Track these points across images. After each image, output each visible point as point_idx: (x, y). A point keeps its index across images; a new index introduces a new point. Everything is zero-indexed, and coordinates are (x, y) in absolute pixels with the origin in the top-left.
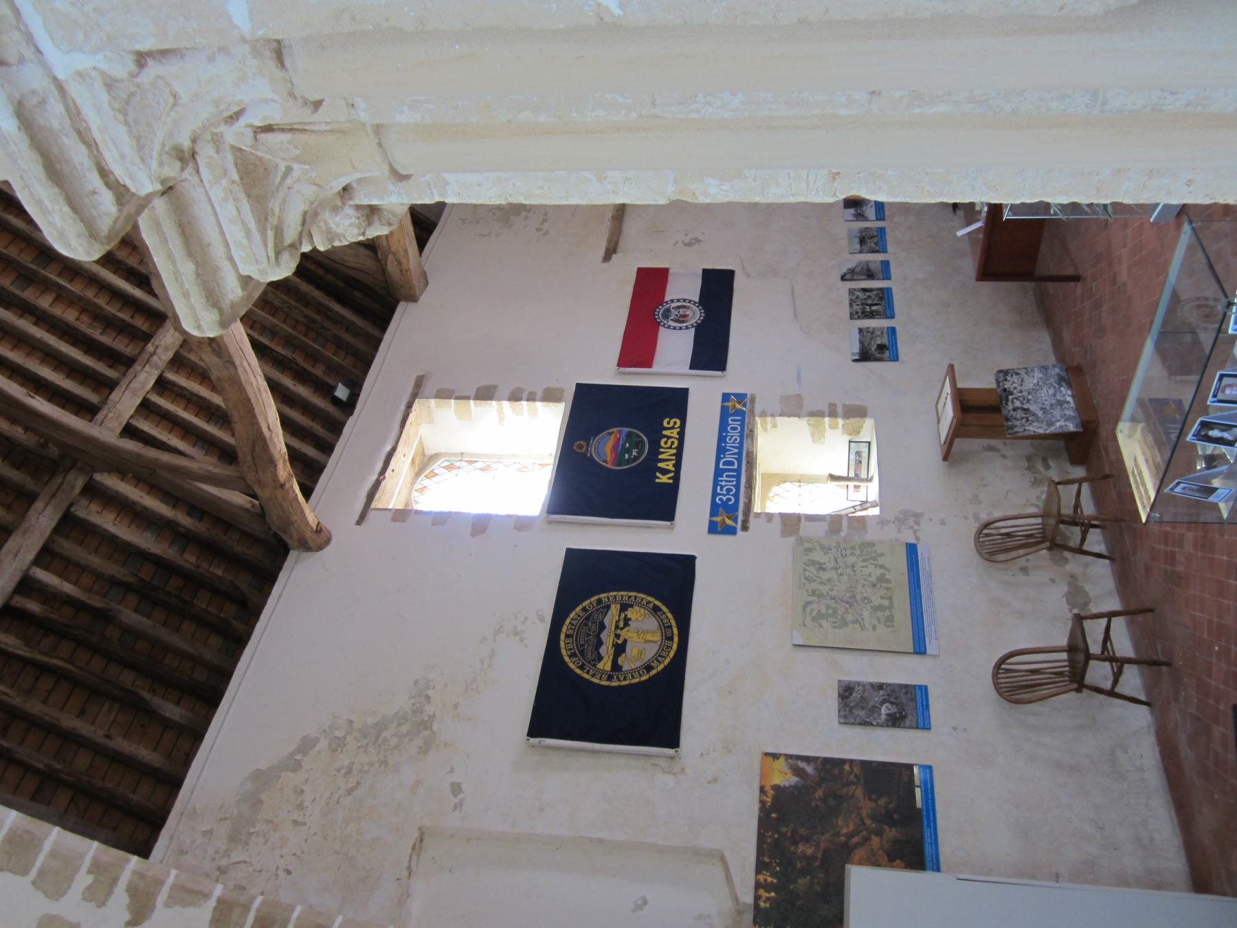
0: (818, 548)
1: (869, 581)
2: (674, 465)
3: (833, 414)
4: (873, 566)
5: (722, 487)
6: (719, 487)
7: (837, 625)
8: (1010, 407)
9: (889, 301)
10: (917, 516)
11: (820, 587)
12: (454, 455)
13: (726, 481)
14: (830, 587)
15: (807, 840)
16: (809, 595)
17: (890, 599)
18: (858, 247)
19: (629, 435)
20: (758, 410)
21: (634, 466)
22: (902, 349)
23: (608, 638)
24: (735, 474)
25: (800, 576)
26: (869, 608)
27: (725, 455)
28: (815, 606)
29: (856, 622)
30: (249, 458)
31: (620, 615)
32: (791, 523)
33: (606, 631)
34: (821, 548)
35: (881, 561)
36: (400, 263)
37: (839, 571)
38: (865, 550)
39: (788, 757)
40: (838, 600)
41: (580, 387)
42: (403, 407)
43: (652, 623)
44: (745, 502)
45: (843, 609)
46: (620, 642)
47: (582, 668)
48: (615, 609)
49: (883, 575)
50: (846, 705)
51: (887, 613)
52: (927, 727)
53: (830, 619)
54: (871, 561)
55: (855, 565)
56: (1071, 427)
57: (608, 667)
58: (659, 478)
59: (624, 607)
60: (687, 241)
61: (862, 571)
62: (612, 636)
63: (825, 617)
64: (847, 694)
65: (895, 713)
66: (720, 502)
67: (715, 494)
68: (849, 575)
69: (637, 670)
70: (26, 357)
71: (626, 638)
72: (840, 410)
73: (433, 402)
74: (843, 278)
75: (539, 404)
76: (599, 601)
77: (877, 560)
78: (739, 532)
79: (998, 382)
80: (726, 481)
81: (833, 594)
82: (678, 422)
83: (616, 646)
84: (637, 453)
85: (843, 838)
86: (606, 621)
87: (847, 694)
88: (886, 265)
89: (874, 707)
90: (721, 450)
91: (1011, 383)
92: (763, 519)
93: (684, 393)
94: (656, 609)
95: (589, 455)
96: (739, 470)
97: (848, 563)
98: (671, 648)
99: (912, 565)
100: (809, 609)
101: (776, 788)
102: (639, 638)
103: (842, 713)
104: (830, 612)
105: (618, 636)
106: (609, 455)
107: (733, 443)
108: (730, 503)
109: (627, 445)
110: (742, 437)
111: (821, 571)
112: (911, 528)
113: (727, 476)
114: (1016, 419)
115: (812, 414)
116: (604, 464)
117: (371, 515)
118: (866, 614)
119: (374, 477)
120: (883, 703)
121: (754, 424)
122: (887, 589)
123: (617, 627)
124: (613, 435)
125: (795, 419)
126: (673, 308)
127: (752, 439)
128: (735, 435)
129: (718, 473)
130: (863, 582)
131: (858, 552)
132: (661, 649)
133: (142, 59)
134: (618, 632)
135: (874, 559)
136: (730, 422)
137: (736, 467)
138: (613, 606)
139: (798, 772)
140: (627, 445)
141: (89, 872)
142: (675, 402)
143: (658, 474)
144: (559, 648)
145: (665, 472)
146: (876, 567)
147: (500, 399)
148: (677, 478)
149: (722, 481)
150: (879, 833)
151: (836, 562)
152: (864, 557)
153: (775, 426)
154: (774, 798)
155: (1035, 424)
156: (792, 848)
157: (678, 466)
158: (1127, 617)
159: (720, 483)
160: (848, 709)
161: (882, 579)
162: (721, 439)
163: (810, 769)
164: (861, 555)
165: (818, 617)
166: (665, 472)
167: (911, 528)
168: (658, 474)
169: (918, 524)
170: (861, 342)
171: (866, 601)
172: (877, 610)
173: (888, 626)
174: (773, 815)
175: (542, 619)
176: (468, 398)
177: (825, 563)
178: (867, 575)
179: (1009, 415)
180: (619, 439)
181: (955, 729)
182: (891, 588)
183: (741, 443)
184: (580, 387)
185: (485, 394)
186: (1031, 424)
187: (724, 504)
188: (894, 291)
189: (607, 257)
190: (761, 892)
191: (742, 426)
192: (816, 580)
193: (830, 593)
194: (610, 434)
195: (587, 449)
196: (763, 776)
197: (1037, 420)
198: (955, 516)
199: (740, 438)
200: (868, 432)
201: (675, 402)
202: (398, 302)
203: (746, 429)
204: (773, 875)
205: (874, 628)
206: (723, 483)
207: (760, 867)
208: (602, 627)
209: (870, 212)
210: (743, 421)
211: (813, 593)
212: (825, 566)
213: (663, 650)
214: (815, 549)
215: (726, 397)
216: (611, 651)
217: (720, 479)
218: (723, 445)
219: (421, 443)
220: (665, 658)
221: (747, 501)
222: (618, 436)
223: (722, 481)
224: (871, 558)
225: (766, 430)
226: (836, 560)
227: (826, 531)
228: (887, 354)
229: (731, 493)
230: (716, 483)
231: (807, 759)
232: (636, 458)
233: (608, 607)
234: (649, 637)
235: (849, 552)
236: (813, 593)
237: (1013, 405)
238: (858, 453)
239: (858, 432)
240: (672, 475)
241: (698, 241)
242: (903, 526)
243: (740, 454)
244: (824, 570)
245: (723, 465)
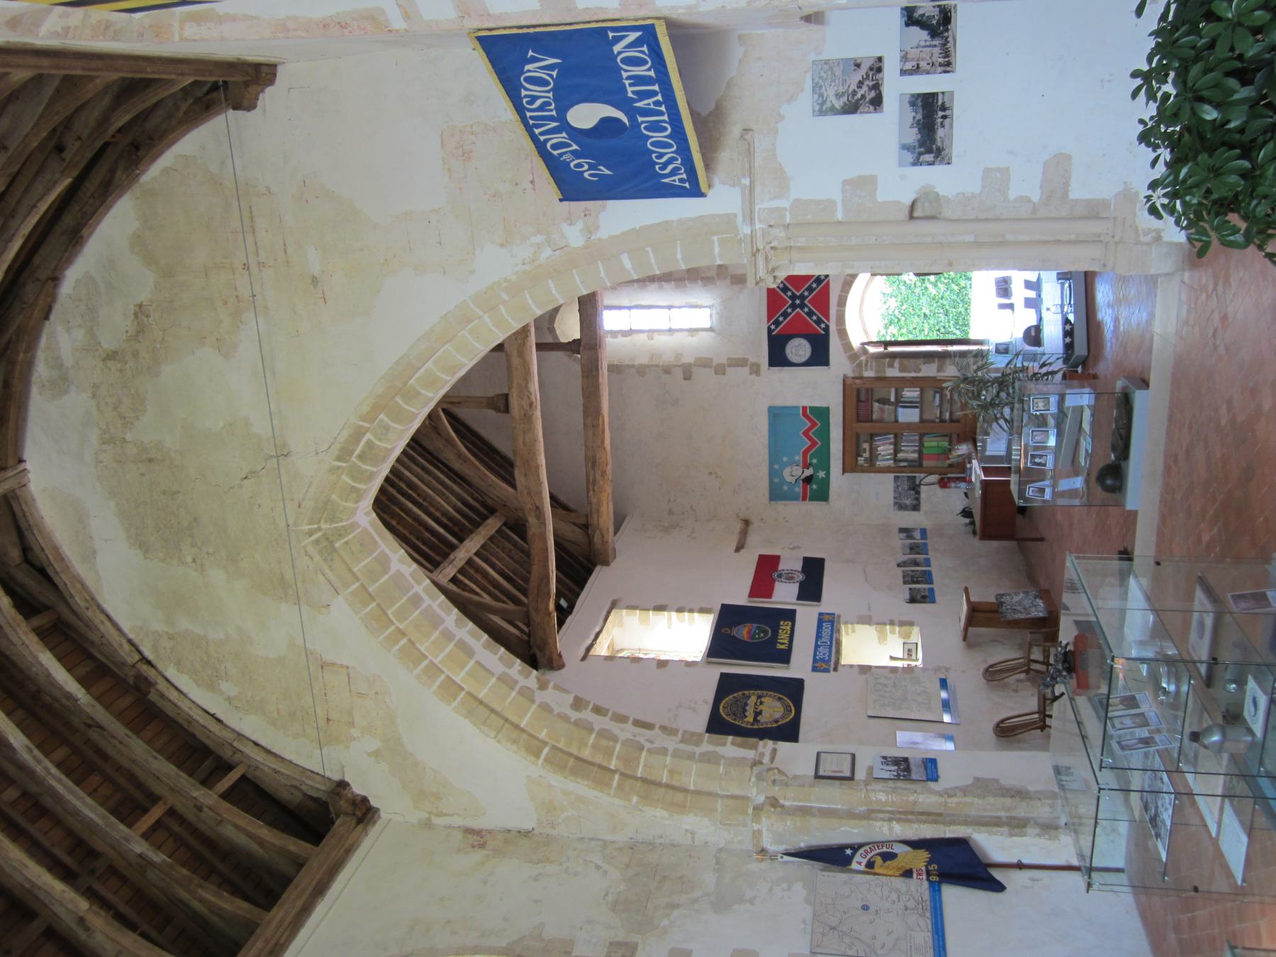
3: (892, 623)
12: (635, 650)
18: (909, 551)
19: (758, 628)
22: (937, 598)
30: (536, 591)
32: (865, 669)
36: (603, 537)
41: (724, 606)
42: (604, 613)
56: (1041, 615)
57: (751, 720)
59: (759, 697)
60: (791, 547)
70: (904, 147)
72: (896, 622)
73: (624, 611)
74: (899, 565)
75: (696, 615)
76: (744, 694)
79: (997, 599)
82: (790, 623)
91: (1006, 599)
93: (794, 611)
94: (780, 699)
115: (878, 624)
117: (588, 657)
119: (589, 642)
125: (867, 626)
133: (770, 226)
142: (790, 615)
147: (670, 610)
153: (853, 631)
176: (648, 610)
184: (724, 606)
185: (660, 608)
188: (933, 572)
189: (738, 549)
200: (916, 636)
201: (790, 615)
202: (595, 566)
208: (746, 704)
209: (917, 535)
215: (821, 614)
216: (753, 715)
219: (612, 639)
225: (847, 634)
228: (928, 599)
230: (816, 650)
238: (909, 650)
239: (908, 636)
241: (799, 547)
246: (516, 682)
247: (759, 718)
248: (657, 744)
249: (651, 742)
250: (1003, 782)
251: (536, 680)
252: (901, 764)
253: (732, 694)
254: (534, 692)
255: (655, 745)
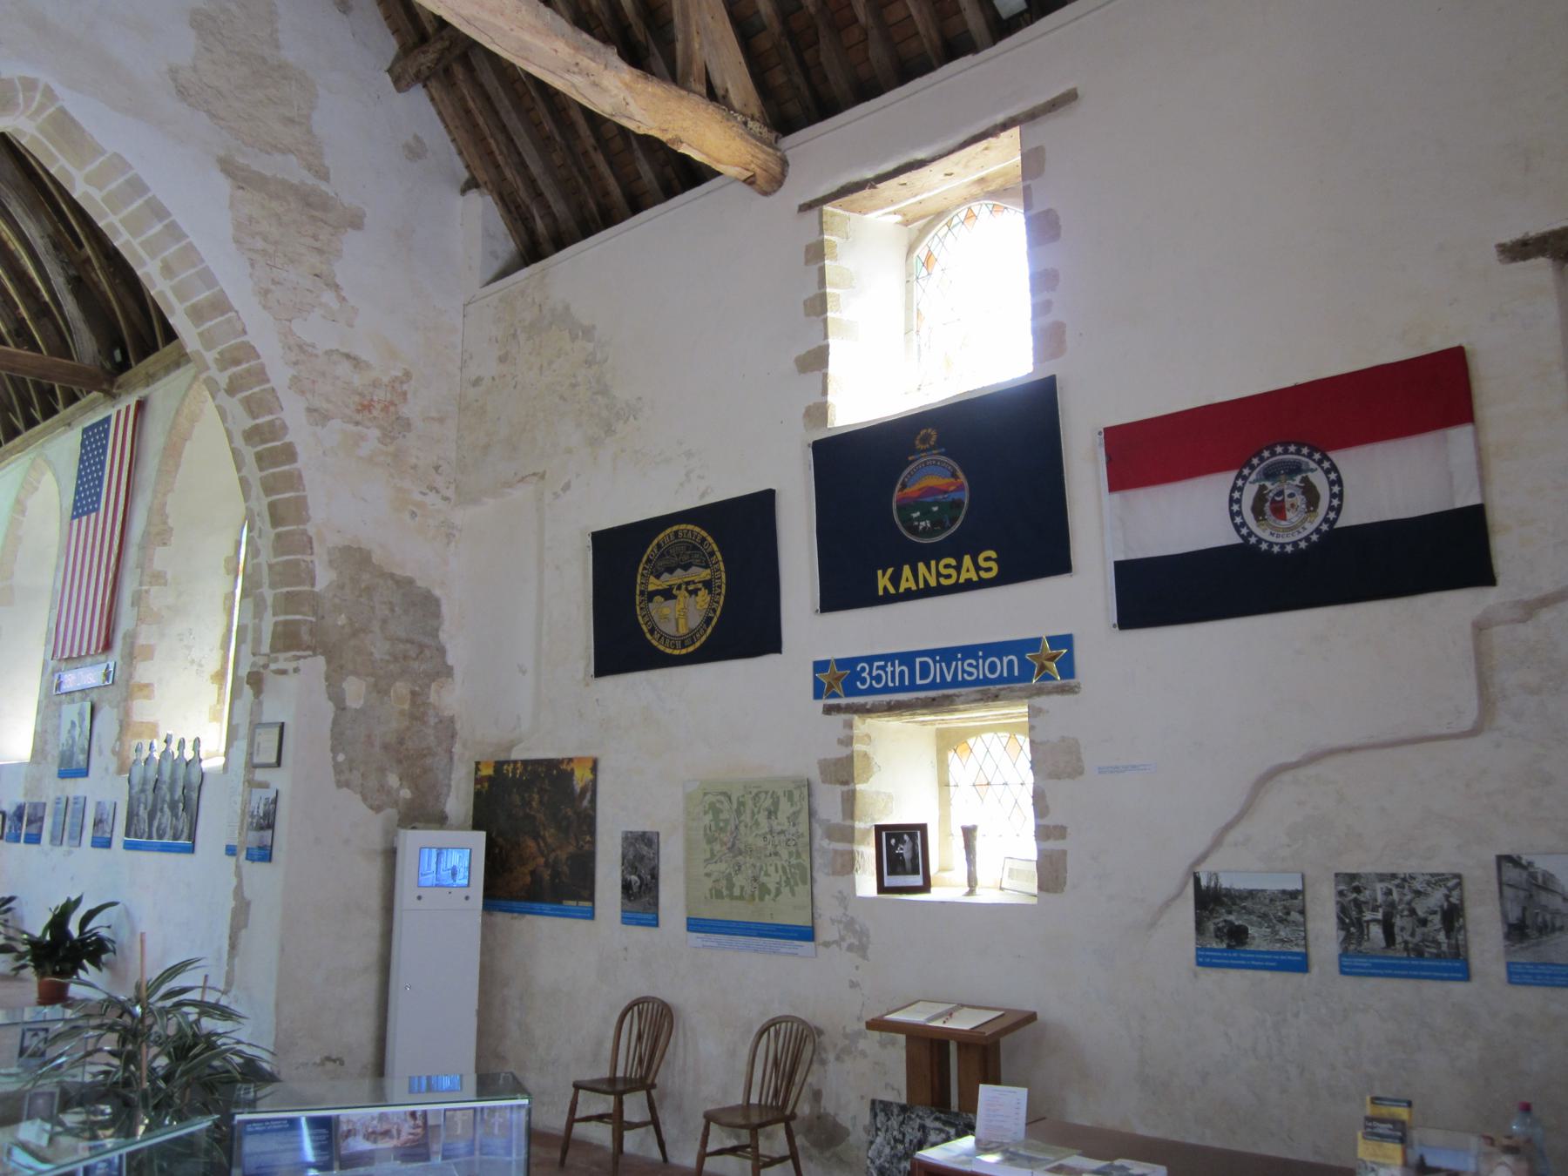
0: (795, 809)
1: (760, 872)
2: (908, 590)
4: (778, 880)
5: (883, 668)
6: (882, 663)
7: (708, 832)
8: (929, 1123)
9: (1401, 967)
10: (861, 949)
11: (748, 812)
13: (893, 673)
14: (750, 824)
15: (541, 802)
16: (738, 799)
17: (741, 898)
20: (1040, 701)
21: (958, 529)
23: (678, 577)
24: (907, 683)
25: (760, 787)
26: (728, 871)
27: (940, 662)
28: (726, 804)
29: (713, 855)
31: (699, 582)
33: (684, 573)
34: (794, 813)
35: (785, 890)
37: (769, 836)
38: (797, 872)
39: (594, 782)
40: (734, 835)
42: (1000, 118)
43: (695, 620)
44: (866, 704)
45: (725, 839)
46: (674, 592)
47: (649, 561)
48: (705, 574)
49: (769, 892)
50: (636, 839)
51: (725, 892)
52: (655, 923)
53: (713, 823)
54: (784, 878)
55: (778, 857)
57: (651, 588)
58: (884, 575)
59: (708, 584)
61: (771, 865)
62: (679, 582)
63: (716, 818)
64: (646, 841)
65: (632, 889)
66: (858, 669)
67: (870, 660)
68: (766, 848)
69: (651, 619)
71: (679, 598)
77: (786, 886)
78: (820, 704)
80: (893, 673)
81: (742, 828)
83: (670, 588)
84: (924, 528)
85: (542, 833)
86: (694, 569)
87: (646, 841)
88: (107, 844)
89: (636, 868)
90: (947, 655)
92: (842, 733)
94: (708, 620)
95: (910, 458)
96: (913, 687)
97: (778, 847)
98: (675, 648)
99: (778, 930)
100: (722, 798)
101: (572, 773)
102: (679, 611)
103: (629, 835)
104: (722, 824)
105: (679, 588)
106: (917, 487)
107: (964, 671)
108: (858, 683)
109: (935, 509)
110: (977, 682)
111: (766, 813)
112: (843, 939)
113: (902, 673)
114: (903, 1123)
116: (898, 486)
118: (723, 866)
119: (869, 174)
120: (640, 877)
121: (1012, 698)
122: (753, 895)
123: (688, 583)
124: (952, 480)
126: (1306, 480)
127: (981, 700)
128: (983, 670)
129: (907, 658)
130: (758, 864)
131: (794, 861)
132: (671, 638)
134: (684, 587)
135: (787, 882)
136: (1005, 660)
137: (919, 682)
138: (708, 571)
139: (584, 791)
140: (935, 509)
141: (219, 353)
143: (890, 571)
144: (664, 529)
145: (895, 581)
146: (777, 883)
148: (888, 599)
149: (893, 665)
150: (546, 864)
151: (779, 833)
152: (788, 868)
154: (565, 772)
155: (887, 1150)
156: (536, 790)
157: (909, 595)
158: (562, 1133)
159: (889, 664)
160: (633, 841)
161: (764, 891)
162: (969, 651)
163: (585, 803)
164: (791, 866)
165: (715, 810)
166: (895, 581)
167: (843, 939)
168: (890, 571)
169: (850, 948)
170: (1251, 894)
171: (737, 868)
172: (727, 880)
173: (711, 890)
174: (555, 772)
175: (703, 496)
177: (776, 818)
178: (766, 871)
179: (913, 1116)
180: (945, 492)
181: (626, 949)
182: (754, 899)
183: (965, 684)
186: (889, 1144)
187: (857, 676)
190: (512, 766)
191: (1000, 680)
192: (756, 806)
193: (743, 824)
194: (954, 475)
195: (923, 451)
196: (581, 760)
197: (895, 1156)
198: (863, 1004)
199: (975, 680)
203: (998, 687)
204: (521, 775)
205: (708, 875)
206: (889, 669)
207: (525, 763)
208: (686, 567)
210: (1011, 679)
211: (741, 804)
212: (773, 817)
213: (671, 640)
214: (792, 805)
216: (665, 586)
217: (897, 662)
218: (959, 656)
220: (663, 645)
221: (868, 707)
222: (952, 488)
223: (893, 665)
224: (787, 878)
226: (782, 832)
227: (829, 821)
229: (874, 682)
231: (593, 801)
232: (914, 530)
233: (707, 567)
234: (682, 622)
235: (793, 849)
236: (741, 804)
237: (936, 1129)
240: (892, 590)
242: (841, 926)
243: (944, 684)
244: (769, 817)
245: (921, 663)
246: (208, 368)
247: (658, 599)
248: (260, 542)
249: (260, 537)
250: (244, 932)
251: (227, 380)
252: (264, 820)
253: (709, 534)
254: (219, 390)
255: (258, 540)
